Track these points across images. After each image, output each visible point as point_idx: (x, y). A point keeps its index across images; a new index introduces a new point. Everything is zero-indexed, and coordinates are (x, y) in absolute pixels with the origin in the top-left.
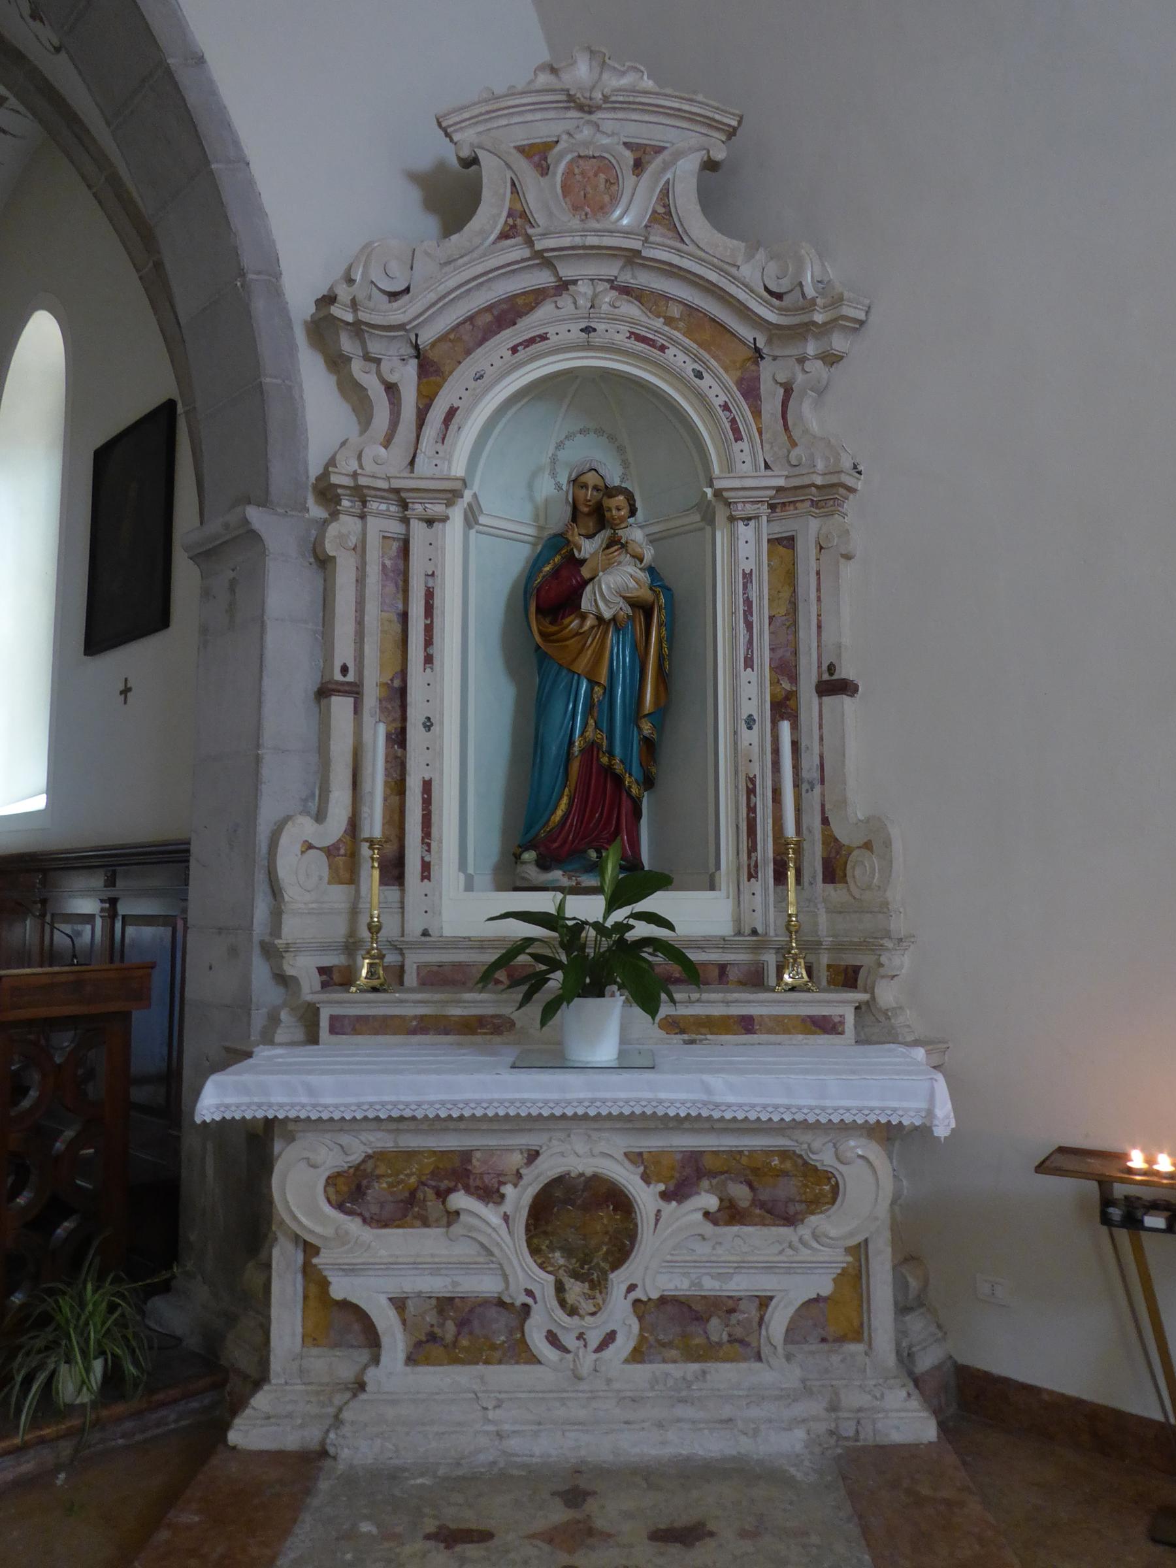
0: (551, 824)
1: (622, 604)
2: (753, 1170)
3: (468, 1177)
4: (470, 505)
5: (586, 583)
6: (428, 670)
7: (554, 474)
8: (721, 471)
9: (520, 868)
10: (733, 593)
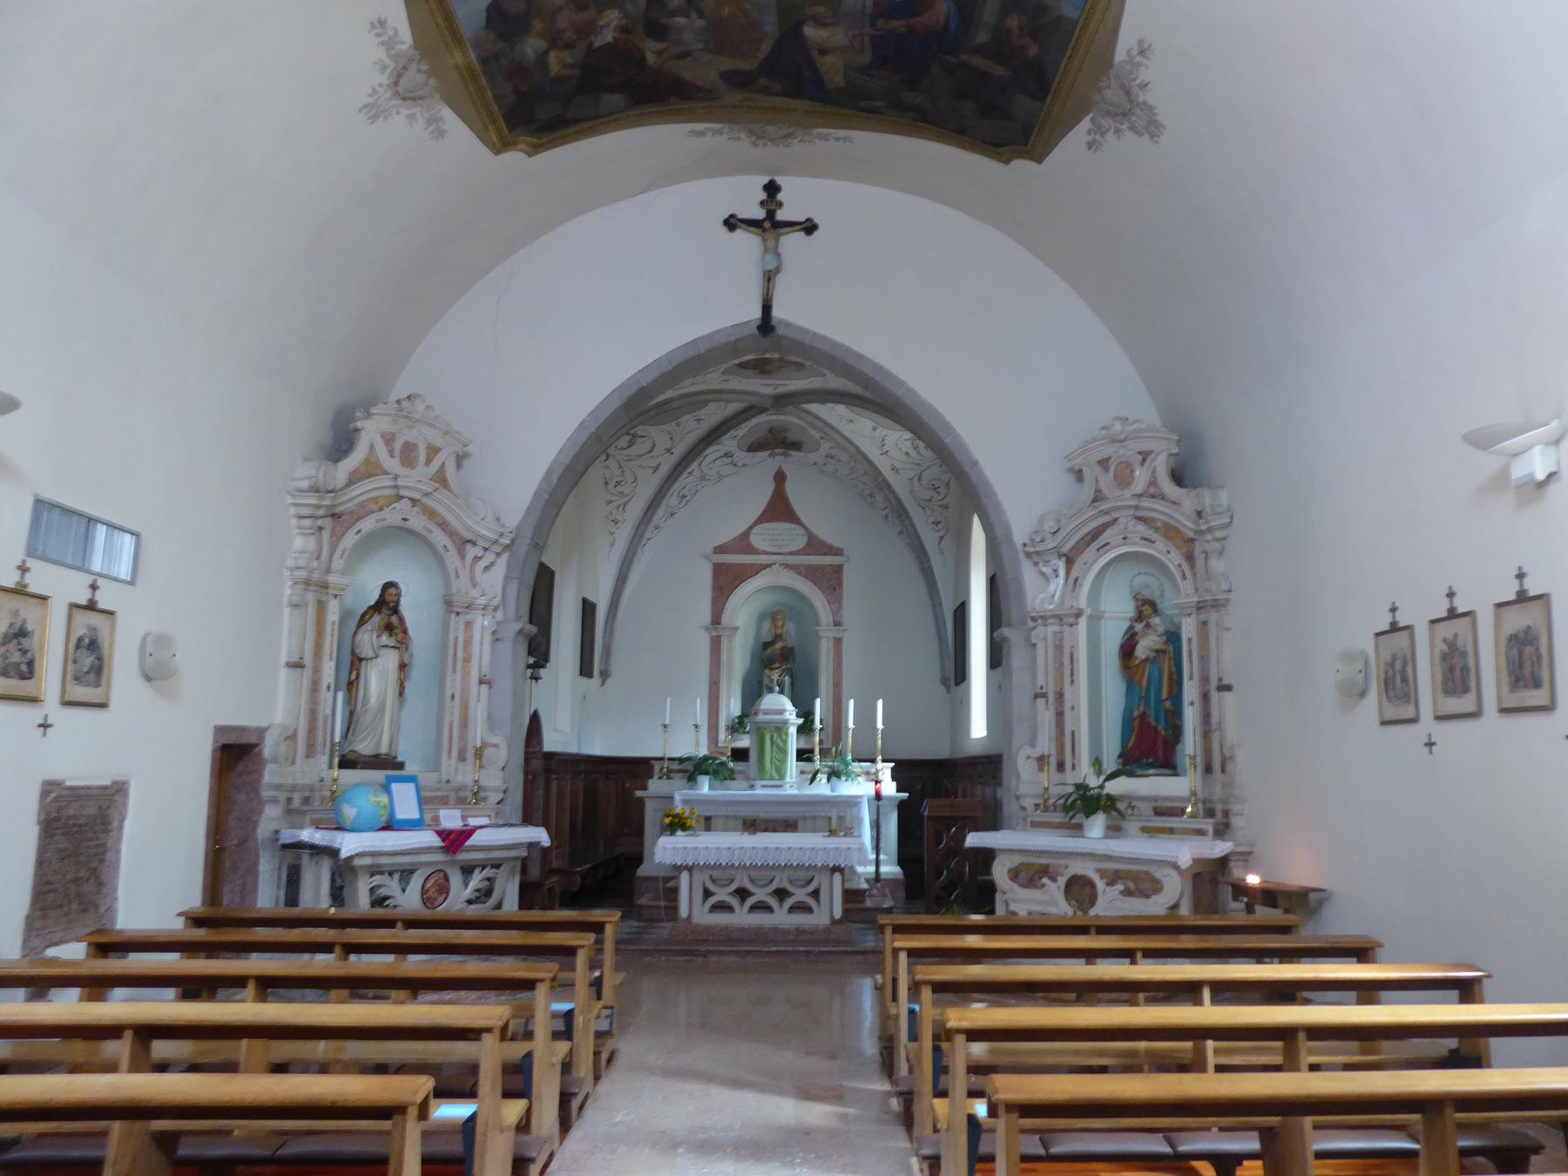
2: (1135, 877)
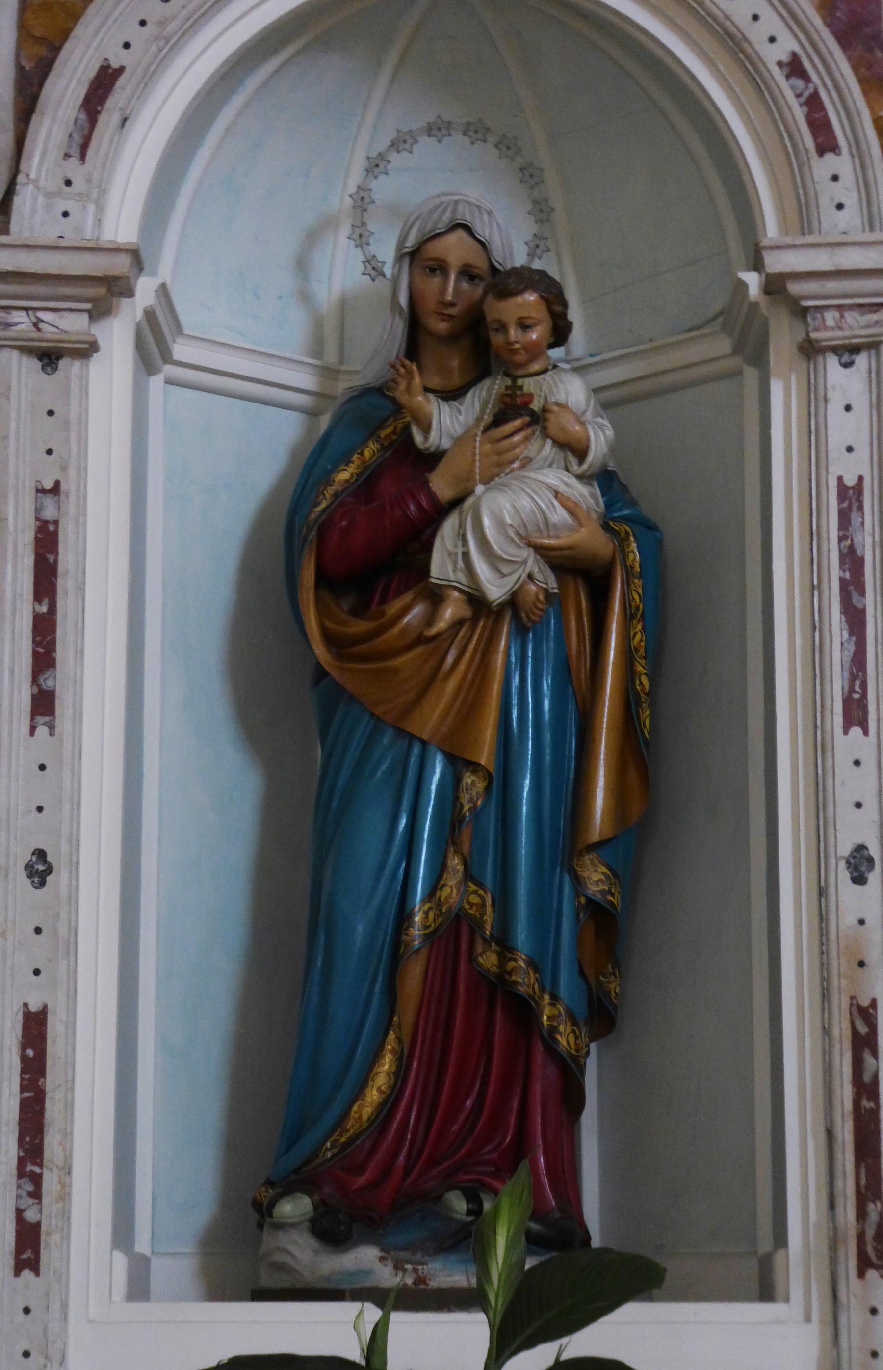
0: (352, 1126)
1: (533, 564)
3: (844, 508)
4: (150, 315)
5: (441, 511)
6: (42, 731)
7: (361, 238)
8: (784, 228)
9: (271, 1240)
10: (813, 535)
